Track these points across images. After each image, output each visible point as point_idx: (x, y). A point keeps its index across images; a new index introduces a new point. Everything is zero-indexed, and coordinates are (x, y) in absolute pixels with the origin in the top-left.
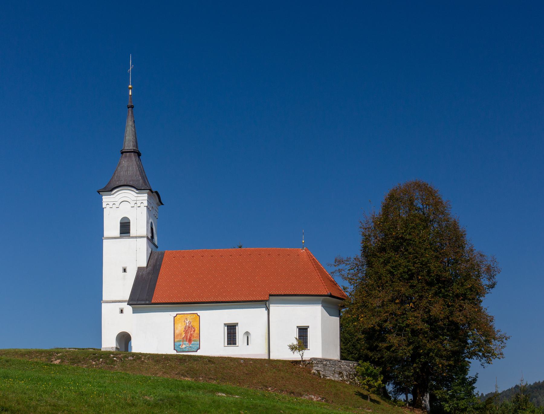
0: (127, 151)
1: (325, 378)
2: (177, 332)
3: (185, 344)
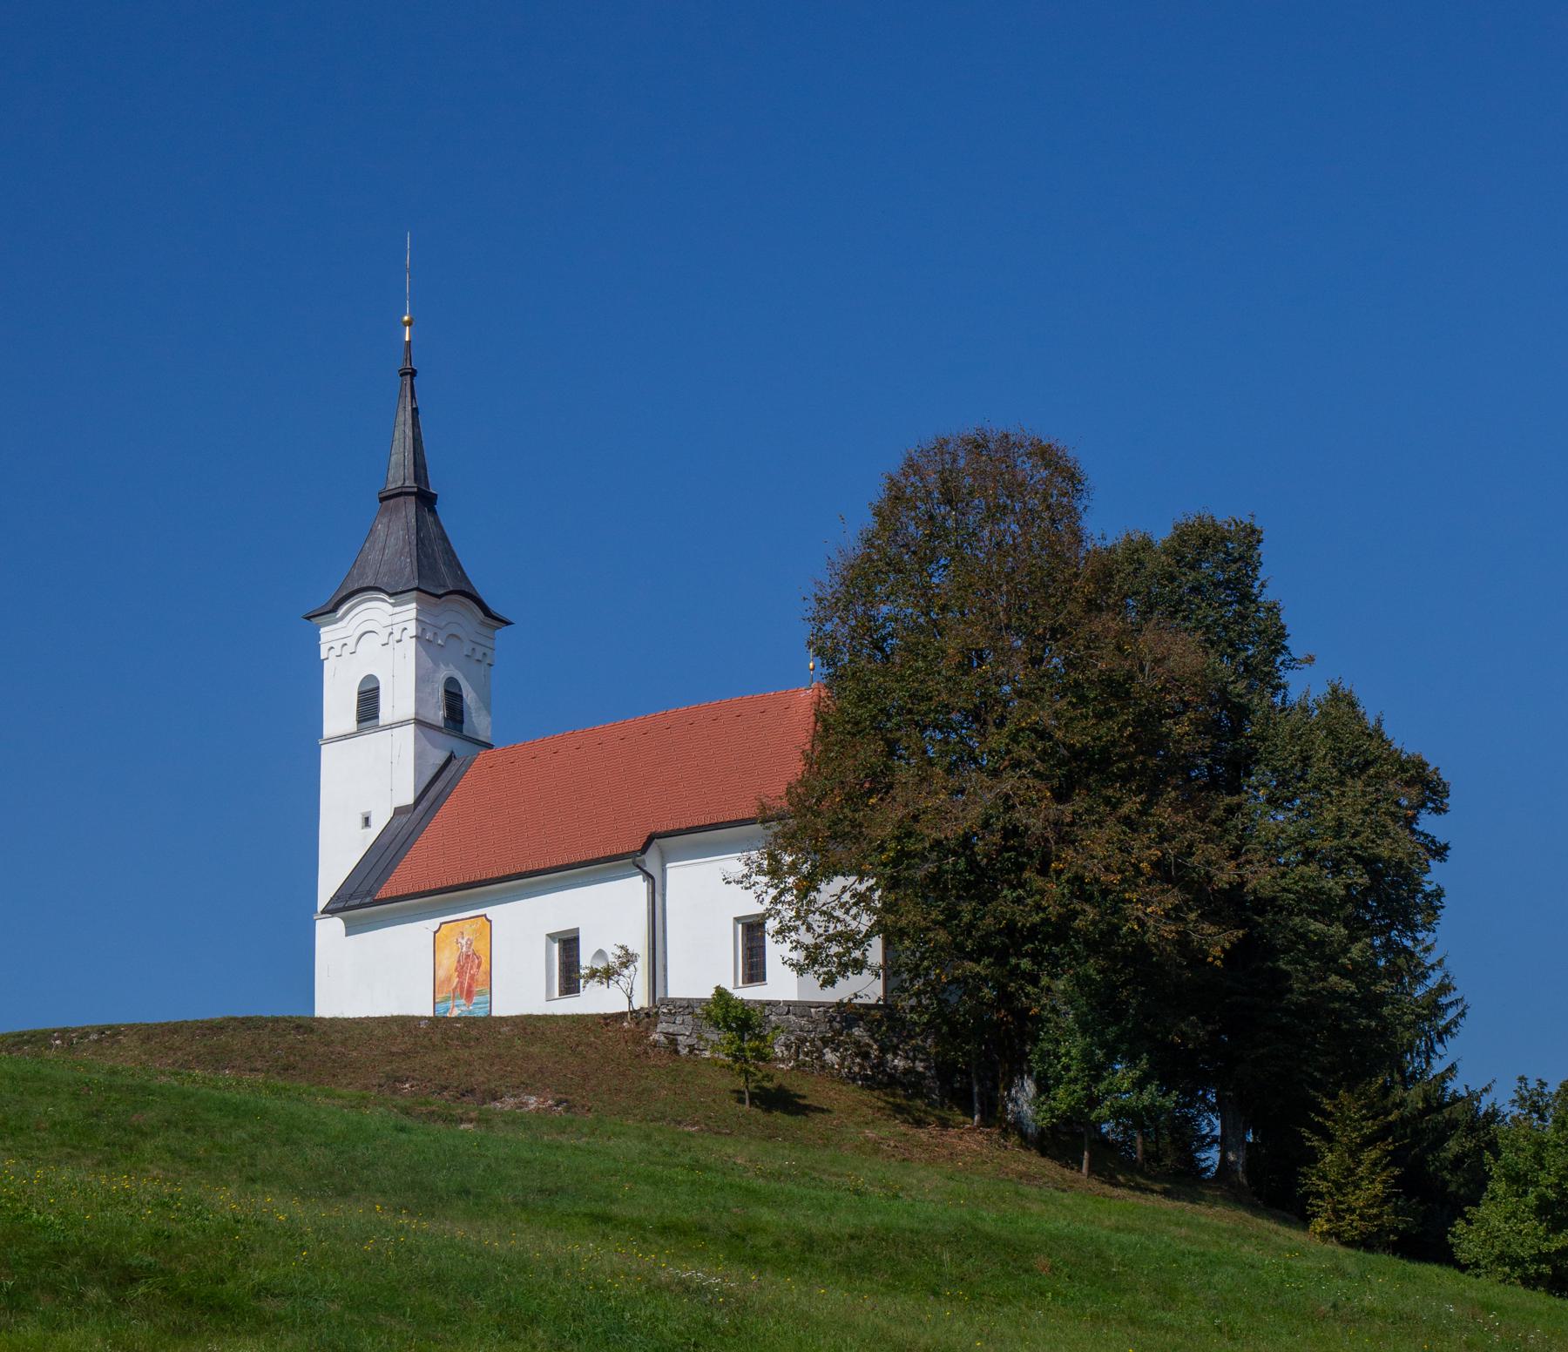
0: (391, 493)
1: (696, 1055)
2: (441, 974)
3: (457, 1006)
